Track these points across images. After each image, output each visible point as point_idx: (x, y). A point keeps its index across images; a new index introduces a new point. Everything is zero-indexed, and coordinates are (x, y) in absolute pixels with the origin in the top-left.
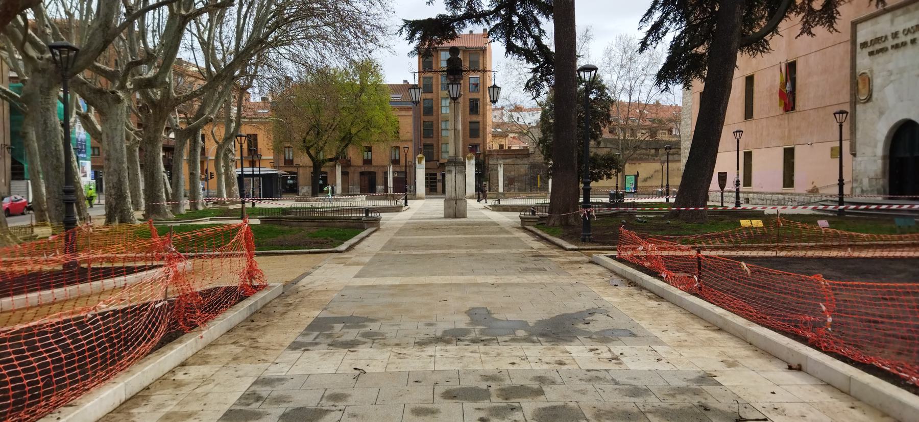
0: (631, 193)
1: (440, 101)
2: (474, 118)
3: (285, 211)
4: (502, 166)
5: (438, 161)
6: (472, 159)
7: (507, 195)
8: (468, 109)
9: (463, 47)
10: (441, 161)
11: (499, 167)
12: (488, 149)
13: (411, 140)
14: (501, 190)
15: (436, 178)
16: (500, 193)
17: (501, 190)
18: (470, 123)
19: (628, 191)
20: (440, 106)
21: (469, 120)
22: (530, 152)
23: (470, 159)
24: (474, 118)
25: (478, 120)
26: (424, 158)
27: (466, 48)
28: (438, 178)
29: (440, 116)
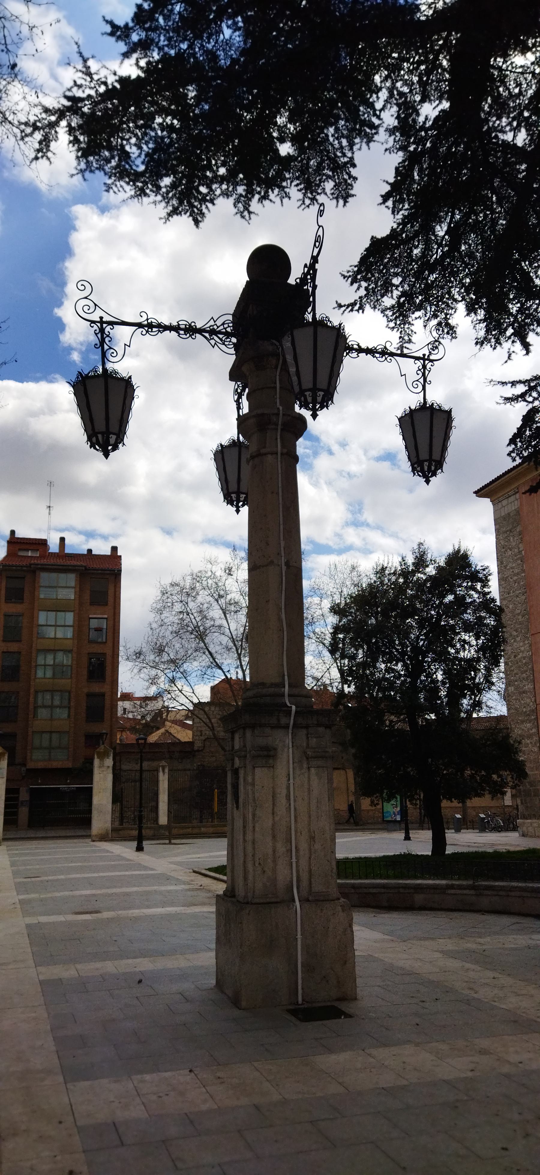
0: (395, 821)
1: (34, 655)
2: (96, 688)
3: (419, 884)
4: (167, 770)
5: (24, 765)
6: (108, 757)
7: (175, 831)
8: (85, 672)
9: (82, 566)
10: (31, 765)
11: (161, 774)
12: (118, 742)
13: (70, 651)
14: (163, 819)
15: (18, 798)
16: (162, 827)
17: (163, 819)
18: (89, 695)
19: (389, 819)
20: (33, 664)
21: (86, 690)
22: (196, 748)
23: (103, 756)
24: (96, 688)
25: (102, 690)
26: (6, 757)
27: (86, 569)
28: (21, 799)
29: (32, 683)
